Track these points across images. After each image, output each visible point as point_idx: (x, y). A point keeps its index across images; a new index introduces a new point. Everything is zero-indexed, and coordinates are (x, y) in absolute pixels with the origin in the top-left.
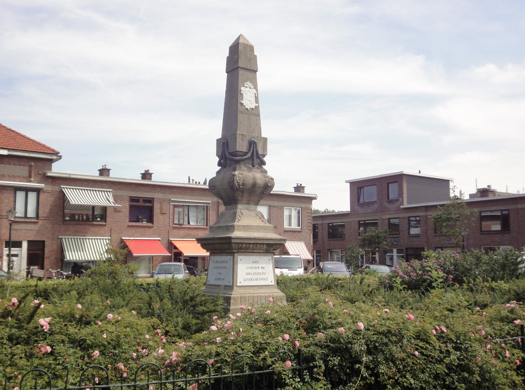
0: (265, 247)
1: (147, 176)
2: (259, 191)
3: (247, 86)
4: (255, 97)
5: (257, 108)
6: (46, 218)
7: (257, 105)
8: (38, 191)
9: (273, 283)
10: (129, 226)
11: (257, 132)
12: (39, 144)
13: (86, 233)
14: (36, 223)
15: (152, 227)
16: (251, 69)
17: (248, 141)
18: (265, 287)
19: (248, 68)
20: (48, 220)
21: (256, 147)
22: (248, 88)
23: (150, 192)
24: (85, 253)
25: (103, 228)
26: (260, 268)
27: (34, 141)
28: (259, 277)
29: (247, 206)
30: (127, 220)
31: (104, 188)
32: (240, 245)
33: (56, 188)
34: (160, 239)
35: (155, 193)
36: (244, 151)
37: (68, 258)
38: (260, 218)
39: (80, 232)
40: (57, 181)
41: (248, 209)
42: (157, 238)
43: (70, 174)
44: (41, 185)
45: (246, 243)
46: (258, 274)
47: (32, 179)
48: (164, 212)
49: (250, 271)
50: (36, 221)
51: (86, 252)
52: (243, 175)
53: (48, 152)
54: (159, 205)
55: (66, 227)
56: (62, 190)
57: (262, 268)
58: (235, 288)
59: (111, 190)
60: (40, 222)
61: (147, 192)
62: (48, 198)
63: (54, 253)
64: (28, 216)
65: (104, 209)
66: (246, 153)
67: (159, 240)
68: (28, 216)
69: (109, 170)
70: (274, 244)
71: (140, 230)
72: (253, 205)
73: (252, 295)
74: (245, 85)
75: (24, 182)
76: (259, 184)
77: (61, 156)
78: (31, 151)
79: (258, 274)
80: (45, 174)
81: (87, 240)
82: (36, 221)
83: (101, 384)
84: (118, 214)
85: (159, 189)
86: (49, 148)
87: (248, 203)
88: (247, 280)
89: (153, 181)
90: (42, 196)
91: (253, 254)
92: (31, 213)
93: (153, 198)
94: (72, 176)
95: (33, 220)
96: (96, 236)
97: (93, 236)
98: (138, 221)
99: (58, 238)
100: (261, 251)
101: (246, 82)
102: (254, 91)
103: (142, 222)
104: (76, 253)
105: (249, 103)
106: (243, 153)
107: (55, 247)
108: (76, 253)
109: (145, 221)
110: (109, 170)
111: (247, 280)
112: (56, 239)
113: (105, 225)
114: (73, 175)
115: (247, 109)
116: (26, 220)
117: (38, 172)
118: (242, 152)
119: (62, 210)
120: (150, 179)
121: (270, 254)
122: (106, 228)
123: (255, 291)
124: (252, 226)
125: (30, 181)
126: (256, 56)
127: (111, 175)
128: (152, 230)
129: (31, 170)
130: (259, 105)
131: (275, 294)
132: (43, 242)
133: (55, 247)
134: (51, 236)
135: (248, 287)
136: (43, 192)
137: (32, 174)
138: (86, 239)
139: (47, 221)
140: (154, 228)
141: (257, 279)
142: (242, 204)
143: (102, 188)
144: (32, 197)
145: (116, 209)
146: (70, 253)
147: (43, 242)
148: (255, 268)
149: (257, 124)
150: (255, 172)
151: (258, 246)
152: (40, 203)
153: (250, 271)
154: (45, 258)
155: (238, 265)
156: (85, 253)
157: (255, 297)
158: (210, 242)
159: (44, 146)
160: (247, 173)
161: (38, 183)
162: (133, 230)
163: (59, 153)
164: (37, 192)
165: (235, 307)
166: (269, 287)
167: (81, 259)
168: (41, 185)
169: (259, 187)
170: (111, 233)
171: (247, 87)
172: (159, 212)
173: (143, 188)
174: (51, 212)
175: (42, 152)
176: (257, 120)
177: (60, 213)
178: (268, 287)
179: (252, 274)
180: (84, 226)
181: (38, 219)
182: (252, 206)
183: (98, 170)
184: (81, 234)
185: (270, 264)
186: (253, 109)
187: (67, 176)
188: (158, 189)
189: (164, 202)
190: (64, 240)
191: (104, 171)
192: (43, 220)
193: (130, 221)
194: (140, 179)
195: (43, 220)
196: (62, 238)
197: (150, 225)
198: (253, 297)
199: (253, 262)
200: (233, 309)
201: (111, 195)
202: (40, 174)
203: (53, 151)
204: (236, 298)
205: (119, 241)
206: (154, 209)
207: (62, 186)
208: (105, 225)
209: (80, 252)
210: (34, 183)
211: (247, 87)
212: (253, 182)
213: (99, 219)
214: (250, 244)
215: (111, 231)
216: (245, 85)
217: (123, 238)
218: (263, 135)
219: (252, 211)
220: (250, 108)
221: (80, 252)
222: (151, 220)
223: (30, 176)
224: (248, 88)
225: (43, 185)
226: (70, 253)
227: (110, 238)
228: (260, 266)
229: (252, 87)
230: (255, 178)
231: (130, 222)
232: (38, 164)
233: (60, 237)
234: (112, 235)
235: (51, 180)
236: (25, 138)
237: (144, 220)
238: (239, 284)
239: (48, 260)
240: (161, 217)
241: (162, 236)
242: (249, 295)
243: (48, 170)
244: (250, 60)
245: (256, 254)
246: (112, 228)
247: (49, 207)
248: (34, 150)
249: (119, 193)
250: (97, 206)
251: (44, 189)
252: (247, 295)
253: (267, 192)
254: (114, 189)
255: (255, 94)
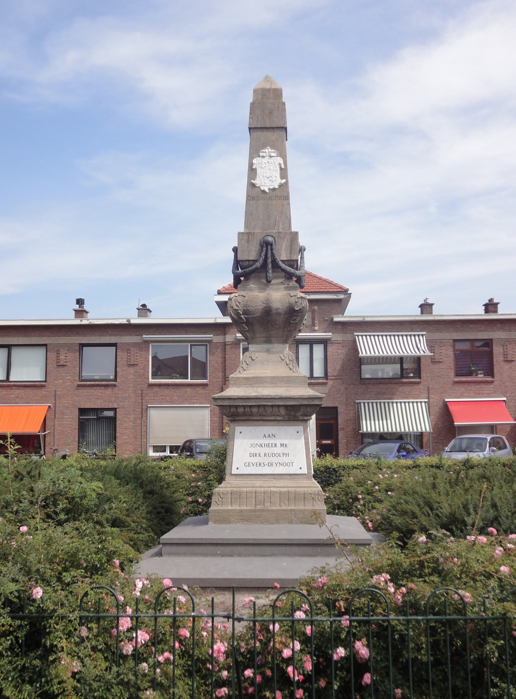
0: (283, 411)
1: (491, 308)
2: (280, 320)
3: (264, 154)
4: (281, 169)
5: (284, 187)
6: (338, 378)
7: (284, 181)
8: (324, 342)
9: (305, 471)
10: (456, 383)
11: (283, 224)
12: (325, 281)
13: (393, 395)
14: (326, 384)
15: (492, 382)
16: (272, 126)
17: (259, 242)
18: (288, 477)
19: (268, 126)
20: (340, 379)
21: (272, 250)
22: (267, 158)
23: (486, 330)
24: (389, 421)
25: (416, 387)
26: (278, 445)
27: (320, 278)
28: (274, 460)
29: (266, 346)
30: (452, 373)
31: (414, 331)
32: (233, 410)
33: (348, 337)
34: (505, 399)
35: (494, 331)
36: (251, 259)
37: (365, 430)
38: (287, 365)
39: (384, 393)
40: (349, 328)
41: (268, 351)
42: (500, 397)
43: (364, 317)
44: (328, 335)
45: (244, 407)
46: (274, 455)
47: (317, 328)
48: (509, 358)
49: (257, 450)
50: (325, 381)
51: (391, 420)
52: (246, 298)
53: (335, 290)
54: (501, 349)
55: (364, 387)
56: (355, 339)
57: (282, 445)
58: (228, 477)
59: (425, 333)
60: (330, 383)
61: (481, 331)
62: (339, 351)
63: (351, 422)
64: (315, 376)
65: (418, 360)
66: (255, 261)
67: (504, 401)
68: (315, 376)
69: (431, 305)
70: (300, 405)
71: (473, 387)
72: (279, 343)
73: (254, 489)
74: (261, 154)
75: (307, 332)
76: (277, 309)
77: (351, 294)
78: (312, 292)
79: (274, 455)
80: (332, 319)
81: (395, 404)
82: (325, 381)
83: (207, 606)
84: (437, 366)
85: (500, 325)
86: (336, 285)
87: (268, 341)
88: (251, 465)
89: (501, 314)
90: (330, 349)
91: (266, 423)
92: (318, 372)
93: (491, 340)
94: (367, 319)
95: (321, 381)
96: (407, 398)
97: (403, 398)
98: (470, 374)
99: (355, 402)
100: (278, 418)
101: (263, 149)
102: (280, 160)
103: (476, 375)
104: (377, 422)
105: (267, 181)
106: (250, 262)
107: (351, 415)
108: (377, 422)
109: (481, 374)
110: (431, 305)
111: (251, 465)
112: (352, 404)
113: (419, 383)
114: (368, 317)
115: (264, 191)
116: (313, 381)
117: (324, 318)
118: (249, 261)
119: (359, 365)
120: (495, 311)
121: (300, 423)
122: (421, 386)
123: (271, 484)
124: (264, 377)
125: (315, 331)
126: (284, 104)
127: (434, 313)
128: (492, 386)
129: (314, 316)
130: (287, 181)
131: (302, 489)
132: (336, 408)
133: (351, 415)
134: (345, 401)
135: (254, 477)
136: (331, 343)
137: (316, 322)
138: (392, 403)
139: (338, 381)
140: (495, 383)
141: (270, 464)
142: (256, 343)
143: (412, 331)
144: (318, 350)
145: (434, 359)
146: (368, 422)
147: (336, 408)
148: (268, 445)
149: (282, 212)
150: (274, 290)
151: (276, 409)
152: (328, 358)
153: (257, 450)
154: (339, 429)
155: (236, 441)
156: (389, 421)
157: (260, 493)
158: (224, 404)
159: (330, 283)
160: (258, 294)
161: (325, 332)
162: (462, 388)
163: (348, 290)
164: (324, 344)
165: (220, 508)
166: (300, 476)
167: (398, 430)
168: (328, 335)
169: (279, 314)
170: (428, 393)
171: (263, 157)
172: (502, 359)
173: (473, 326)
174: (343, 368)
175: (326, 292)
176: (283, 205)
177: (355, 369)
178: (294, 476)
179: (262, 455)
180: (389, 385)
181: (327, 379)
182: (276, 345)
183: (483, 305)
184: (385, 396)
185: (299, 438)
186: (274, 189)
187: (360, 319)
188: (498, 325)
189: (510, 344)
190: (362, 405)
191: (426, 307)
192: (333, 379)
193: (457, 375)
194: (483, 312)
195: (333, 379)
196: (360, 403)
197: (489, 379)
198: (255, 492)
199: (265, 436)
200: (214, 511)
201: (423, 340)
202: (327, 320)
203: (340, 288)
204: (223, 493)
205: (441, 404)
206: (494, 355)
207: (355, 334)
208: (492, 382)
209: (374, 420)
210: (320, 332)
211: (263, 157)
212: (265, 307)
213: (412, 375)
214: (251, 406)
215: (428, 390)
216: (261, 154)
217: (446, 400)
218: (294, 229)
219: (274, 353)
220: (269, 189)
221: (374, 420)
222: (490, 372)
223: (314, 325)
224: (267, 158)
225: (331, 334)
226: (368, 422)
227: (427, 400)
228: (278, 442)
229: (273, 154)
230: (268, 300)
231: (457, 376)
232: (323, 307)
233: (357, 401)
234: (430, 396)
235: (341, 327)
236: (311, 275)
237: (479, 372)
238: (234, 471)
239: (343, 432)
240: (506, 366)
241: (508, 395)
242: (250, 489)
243: (335, 314)
244: (271, 113)
245: (270, 423)
246: (430, 386)
247: (340, 363)
248: (315, 290)
249: (437, 336)
250: (407, 357)
251: (332, 339)
252: (245, 490)
253: (295, 320)
254: (429, 331)
255: (280, 164)
